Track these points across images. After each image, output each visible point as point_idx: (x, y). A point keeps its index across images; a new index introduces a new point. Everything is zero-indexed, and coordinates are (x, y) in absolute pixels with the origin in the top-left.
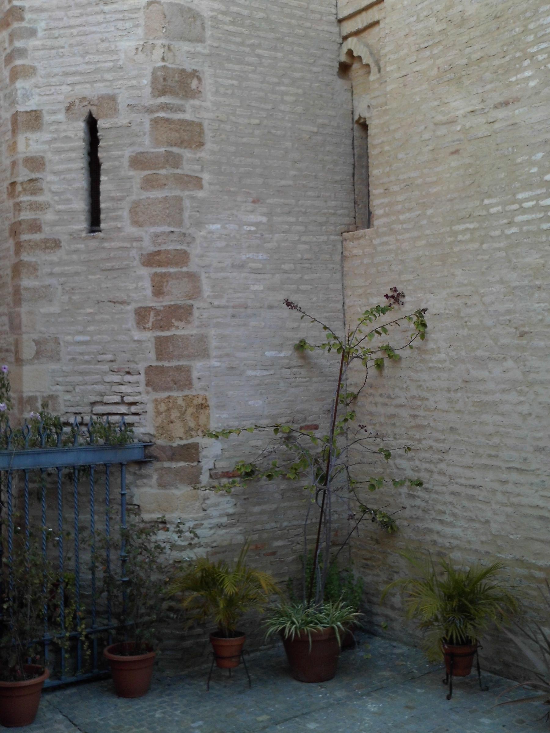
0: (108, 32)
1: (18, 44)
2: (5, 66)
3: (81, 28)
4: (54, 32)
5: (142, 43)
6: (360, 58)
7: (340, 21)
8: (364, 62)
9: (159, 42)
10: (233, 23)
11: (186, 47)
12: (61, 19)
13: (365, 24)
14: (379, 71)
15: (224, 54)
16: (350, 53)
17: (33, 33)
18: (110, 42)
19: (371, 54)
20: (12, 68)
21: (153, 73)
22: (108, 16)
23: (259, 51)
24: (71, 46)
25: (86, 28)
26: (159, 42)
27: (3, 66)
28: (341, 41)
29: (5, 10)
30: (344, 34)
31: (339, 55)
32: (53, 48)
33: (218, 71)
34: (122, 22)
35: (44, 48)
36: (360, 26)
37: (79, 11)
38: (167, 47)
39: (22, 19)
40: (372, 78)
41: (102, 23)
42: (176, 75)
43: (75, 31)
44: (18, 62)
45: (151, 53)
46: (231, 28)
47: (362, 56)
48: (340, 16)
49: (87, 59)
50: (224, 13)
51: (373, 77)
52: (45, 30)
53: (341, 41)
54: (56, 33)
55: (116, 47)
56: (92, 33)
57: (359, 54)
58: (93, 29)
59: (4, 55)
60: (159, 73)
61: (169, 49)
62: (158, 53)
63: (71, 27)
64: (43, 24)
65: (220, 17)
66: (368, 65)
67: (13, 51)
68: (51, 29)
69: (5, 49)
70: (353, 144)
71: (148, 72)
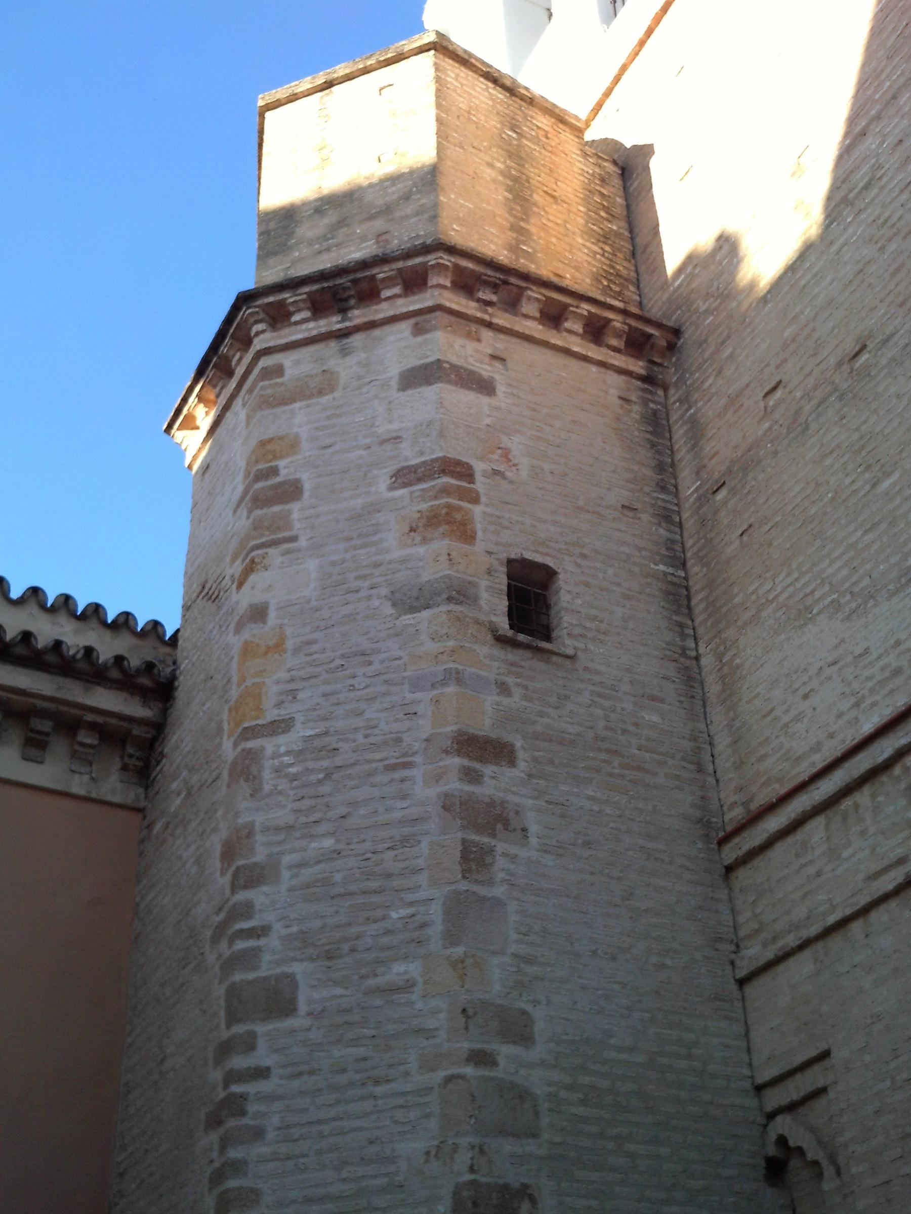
0: (378, 1128)
1: (234, 1153)
2: (210, 1189)
3: (337, 1123)
4: (292, 1131)
5: (436, 1143)
6: (800, 1151)
7: (759, 1089)
8: (810, 1156)
9: (464, 1141)
10: (584, 1102)
11: (508, 1146)
12: (305, 1110)
13: (802, 1093)
14: (838, 1173)
15: (572, 1154)
16: (782, 1141)
17: (258, 1134)
18: (382, 1142)
19: (820, 1142)
20: (221, 1193)
21: (455, 1193)
22: (380, 1102)
23: (630, 1147)
24: (319, 1152)
25: (344, 1123)
26: (464, 1141)
27: (206, 1189)
28: (764, 1122)
29: (217, 1100)
30: (769, 1109)
31: (763, 1146)
32: (289, 1158)
33: (563, 1185)
34: (402, 1110)
35: (275, 1158)
36: (795, 1097)
37: (334, 1096)
38: (477, 1149)
39: (243, 1113)
40: (827, 1186)
41: (371, 1113)
42: (494, 1194)
43: (326, 1129)
44: (232, 1183)
45: (452, 1159)
46: (582, 1111)
47: (805, 1146)
48: (759, 1081)
49: (344, 1174)
50: (570, 1088)
51: (829, 1184)
52: (279, 1129)
53: (764, 1122)
54: (296, 1132)
55: (393, 1150)
56: (353, 1130)
57: (799, 1144)
58: (357, 1123)
59: (209, 1172)
60: (465, 1193)
61: (482, 1151)
62: (463, 1159)
63: (320, 1122)
64: (275, 1120)
65: (563, 1094)
66: (816, 1163)
67: (224, 1165)
68: (288, 1127)
69: (212, 1161)
70: (704, 706)
71: (446, 1192)
